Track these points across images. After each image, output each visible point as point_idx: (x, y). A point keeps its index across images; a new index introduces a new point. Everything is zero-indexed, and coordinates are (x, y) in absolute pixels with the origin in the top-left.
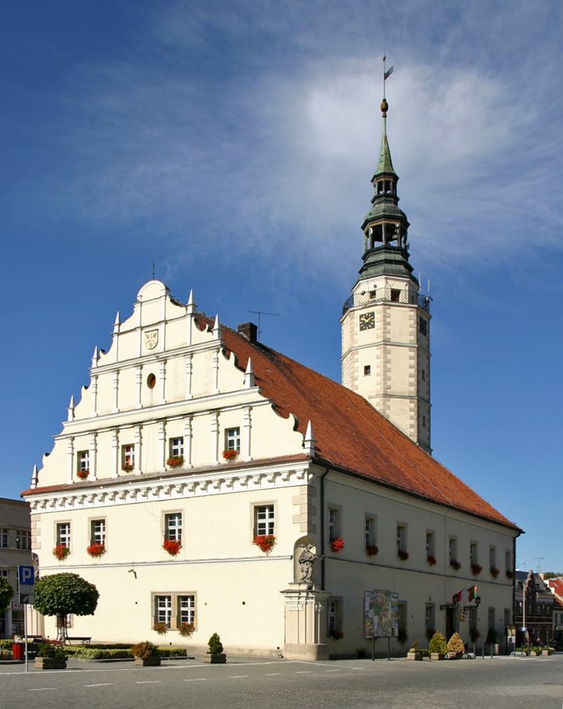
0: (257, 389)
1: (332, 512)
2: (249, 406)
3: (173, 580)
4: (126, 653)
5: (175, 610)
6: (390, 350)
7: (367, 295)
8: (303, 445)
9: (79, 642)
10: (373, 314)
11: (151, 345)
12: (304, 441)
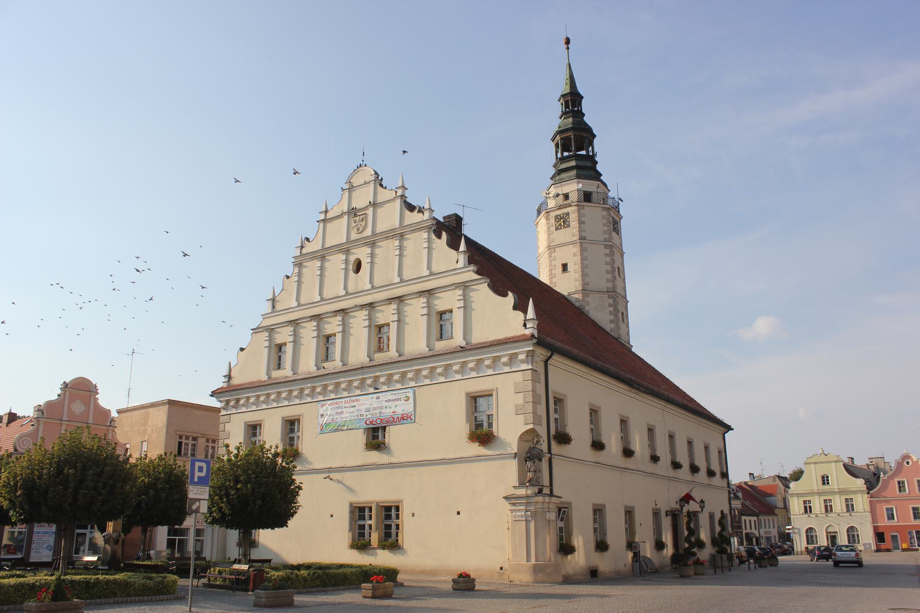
0: (472, 268)
1: (555, 403)
2: (465, 286)
3: (374, 490)
4: (9, 553)
5: (377, 524)
7: (561, 197)
8: (525, 325)
9: (546, 482)
10: (568, 214)
11: (358, 229)
12: (525, 320)
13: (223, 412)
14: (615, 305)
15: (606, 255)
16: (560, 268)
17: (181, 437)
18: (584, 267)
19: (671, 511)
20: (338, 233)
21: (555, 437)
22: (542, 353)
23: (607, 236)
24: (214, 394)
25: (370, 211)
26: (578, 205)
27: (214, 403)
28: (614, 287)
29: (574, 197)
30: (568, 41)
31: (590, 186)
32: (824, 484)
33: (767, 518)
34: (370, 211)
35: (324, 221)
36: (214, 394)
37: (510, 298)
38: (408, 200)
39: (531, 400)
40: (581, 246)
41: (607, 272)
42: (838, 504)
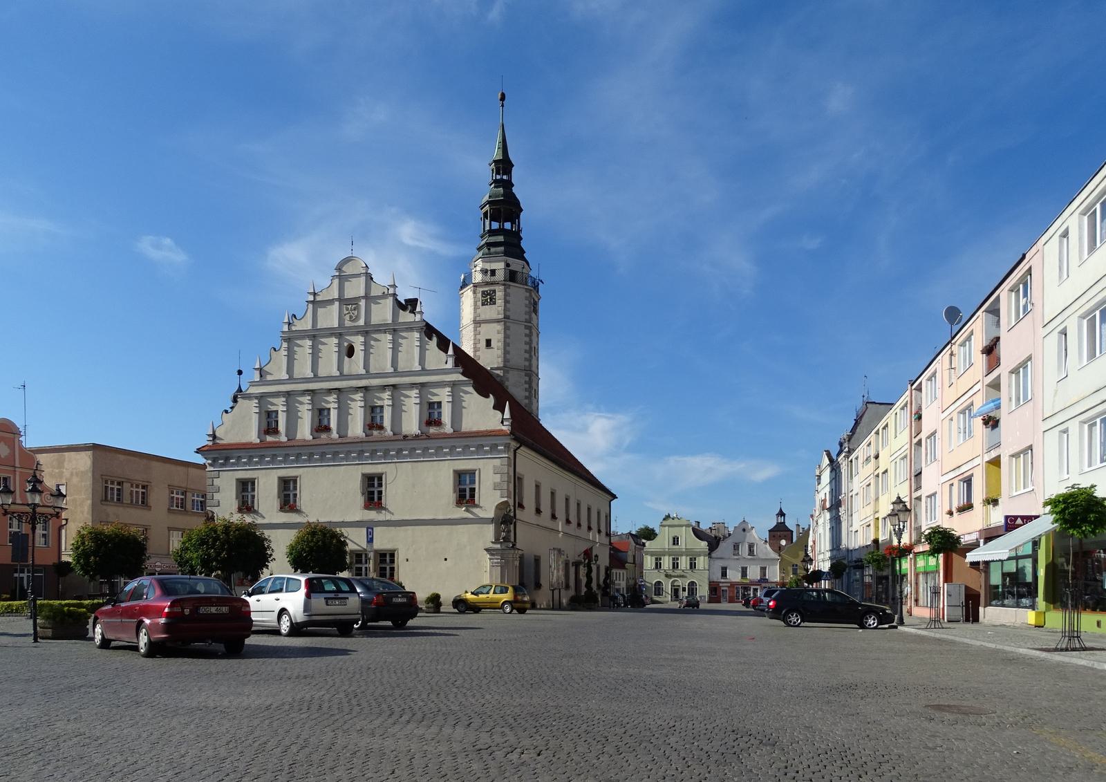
2: (454, 385)
6: (509, 327)
8: (502, 422)
11: (351, 317)
13: (209, 468)
14: (530, 383)
15: (526, 335)
16: (484, 343)
17: (106, 482)
18: (506, 344)
19: (575, 562)
20: (330, 318)
21: (812, 560)
22: (514, 444)
23: (527, 317)
24: (199, 451)
25: (362, 303)
26: (504, 285)
27: (200, 459)
28: (530, 365)
29: (500, 276)
30: (503, 98)
31: (516, 264)
32: (674, 544)
33: (618, 571)
34: (362, 303)
35: (313, 302)
36: (199, 451)
37: (491, 400)
38: (398, 298)
39: (506, 479)
40: (505, 324)
41: (526, 351)
42: (684, 562)
